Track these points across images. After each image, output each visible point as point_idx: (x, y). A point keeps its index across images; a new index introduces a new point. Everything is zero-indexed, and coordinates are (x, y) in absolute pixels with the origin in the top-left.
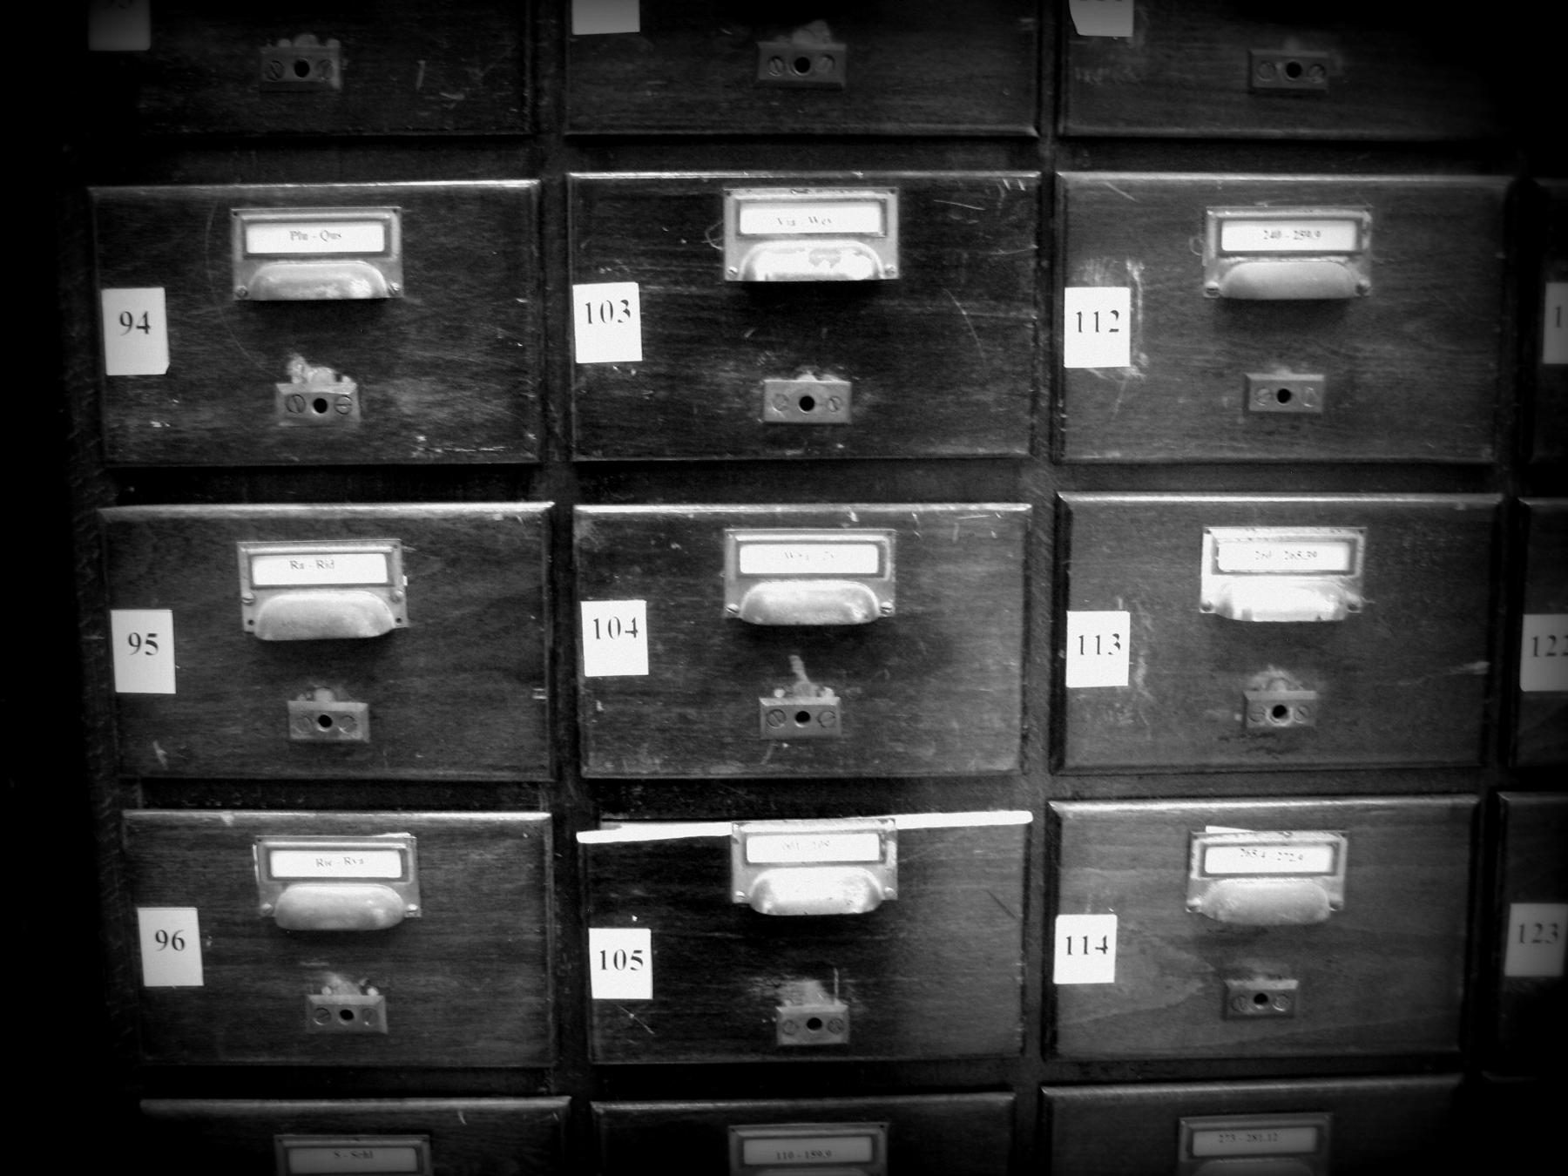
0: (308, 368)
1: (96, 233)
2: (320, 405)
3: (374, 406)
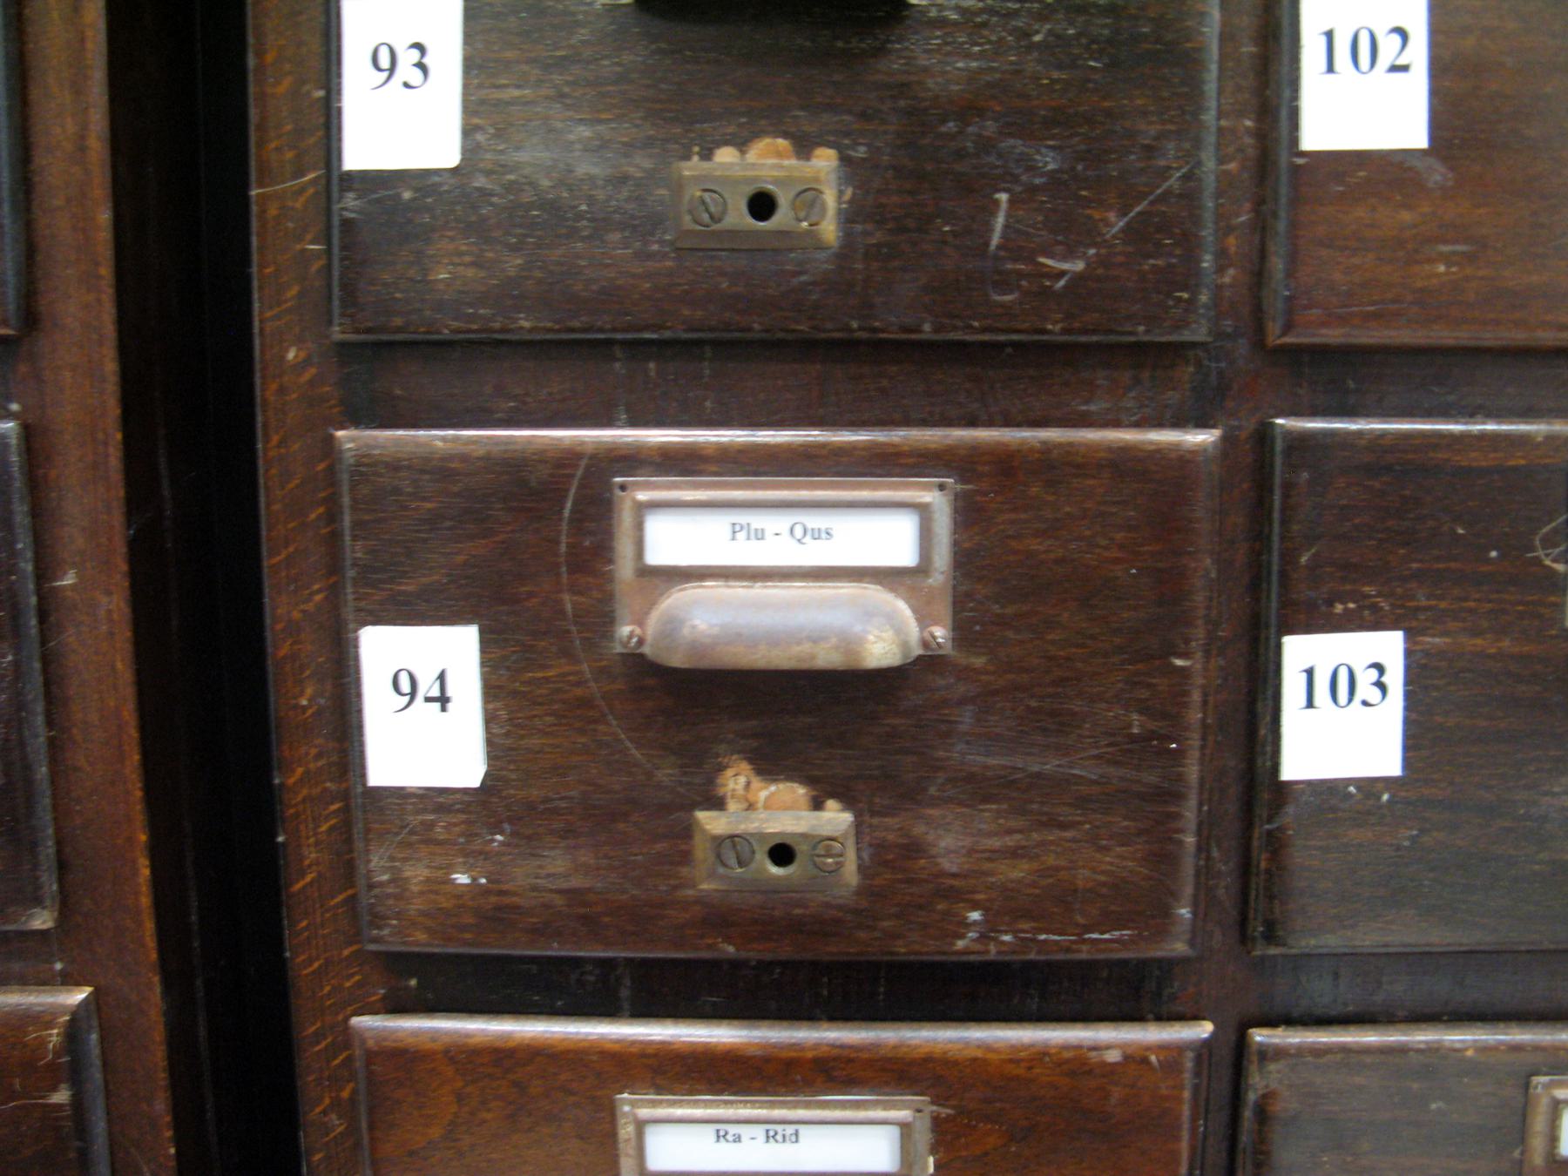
0: (757, 783)
1: (347, 520)
2: (782, 853)
3: (891, 861)
